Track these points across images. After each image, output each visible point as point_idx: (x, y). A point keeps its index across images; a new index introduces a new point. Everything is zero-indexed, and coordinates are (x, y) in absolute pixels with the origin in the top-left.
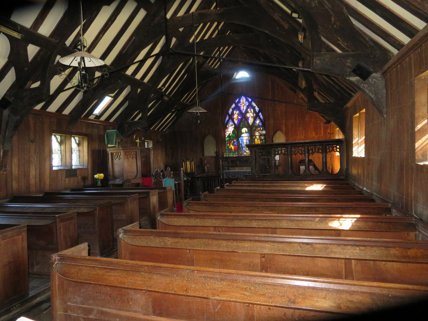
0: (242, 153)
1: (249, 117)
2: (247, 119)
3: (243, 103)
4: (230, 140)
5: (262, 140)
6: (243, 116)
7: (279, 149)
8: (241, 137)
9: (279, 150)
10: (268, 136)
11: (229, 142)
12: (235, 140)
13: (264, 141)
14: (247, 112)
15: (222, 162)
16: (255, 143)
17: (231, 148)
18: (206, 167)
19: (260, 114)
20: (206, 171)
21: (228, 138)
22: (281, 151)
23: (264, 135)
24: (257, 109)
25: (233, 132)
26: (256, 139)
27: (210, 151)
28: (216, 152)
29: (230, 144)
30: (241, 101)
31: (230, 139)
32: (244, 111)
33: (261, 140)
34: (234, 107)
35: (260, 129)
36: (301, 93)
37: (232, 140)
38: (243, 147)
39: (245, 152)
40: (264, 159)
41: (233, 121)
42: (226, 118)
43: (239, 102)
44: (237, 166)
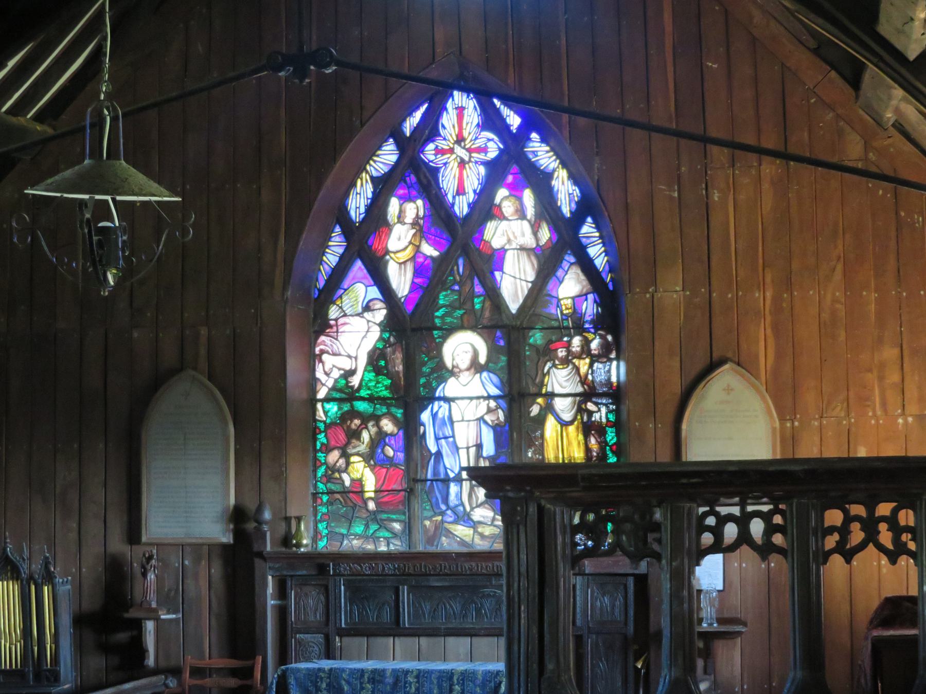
0: (440, 530)
1: (502, 252)
2: (487, 264)
3: (463, 138)
4: (345, 417)
5: (600, 430)
6: (459, 239)
7: (723, 510)
8: (432, 399)
9: (723, 520)
10: (651, 402)
11: (347, 428)
12: (388, 426)
13: (611, 436)
14: (484, 209)
15: (282, 592)
16: (541, 449)
17: (358, 483)
18: (150, 626)
19: (588, 229)
20: (151, 661)
21: (333, 408)
22: (743, 521)
23: (615, 394)
24: (566, 191)
25: (376, 360)
26: (551, 425)
27: (190, 502)
28: (238, 516)
29: (345, 455)
30: (448, 120)
31: (353, 414)
32: (461, 207)
33: (589, 428)
34: (394, 168)
35: (586, 343)
36: (899, 92)
37: (366, 419)
38: (446, 481)
39: (465, 518)
40: (605, 580)
41: (379, 278)
42: (323, 246)
43: (430, 129)
44: (395, 630)
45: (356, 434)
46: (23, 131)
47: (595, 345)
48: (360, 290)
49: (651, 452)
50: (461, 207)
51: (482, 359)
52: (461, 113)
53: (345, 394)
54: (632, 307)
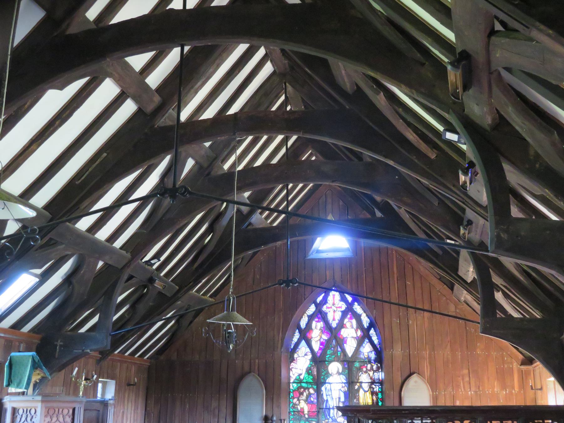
2: (341, 342)
6: (334, 334)
8: (325, 383)
11: (299, 392)
13: (380, 396)
14: (341, 325)
17: (302, 410)
19: (372, 332)
21: (295, 385)
23: (381, 383)
30: (330, 298)
32: (334, 325)
33: (373, 393)
36: (465, 292)
43: (325, 301)
45: (302, 394)
46: (206, 300)
47: (375, 367)
48: (303, 348)
49: (392, 403)
50: (334, 325)
51: (340, 371)
52: (334, 297)
53: (299, 381)
54: (386, 355)
